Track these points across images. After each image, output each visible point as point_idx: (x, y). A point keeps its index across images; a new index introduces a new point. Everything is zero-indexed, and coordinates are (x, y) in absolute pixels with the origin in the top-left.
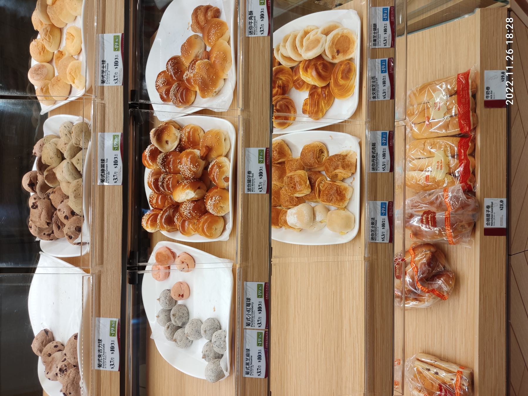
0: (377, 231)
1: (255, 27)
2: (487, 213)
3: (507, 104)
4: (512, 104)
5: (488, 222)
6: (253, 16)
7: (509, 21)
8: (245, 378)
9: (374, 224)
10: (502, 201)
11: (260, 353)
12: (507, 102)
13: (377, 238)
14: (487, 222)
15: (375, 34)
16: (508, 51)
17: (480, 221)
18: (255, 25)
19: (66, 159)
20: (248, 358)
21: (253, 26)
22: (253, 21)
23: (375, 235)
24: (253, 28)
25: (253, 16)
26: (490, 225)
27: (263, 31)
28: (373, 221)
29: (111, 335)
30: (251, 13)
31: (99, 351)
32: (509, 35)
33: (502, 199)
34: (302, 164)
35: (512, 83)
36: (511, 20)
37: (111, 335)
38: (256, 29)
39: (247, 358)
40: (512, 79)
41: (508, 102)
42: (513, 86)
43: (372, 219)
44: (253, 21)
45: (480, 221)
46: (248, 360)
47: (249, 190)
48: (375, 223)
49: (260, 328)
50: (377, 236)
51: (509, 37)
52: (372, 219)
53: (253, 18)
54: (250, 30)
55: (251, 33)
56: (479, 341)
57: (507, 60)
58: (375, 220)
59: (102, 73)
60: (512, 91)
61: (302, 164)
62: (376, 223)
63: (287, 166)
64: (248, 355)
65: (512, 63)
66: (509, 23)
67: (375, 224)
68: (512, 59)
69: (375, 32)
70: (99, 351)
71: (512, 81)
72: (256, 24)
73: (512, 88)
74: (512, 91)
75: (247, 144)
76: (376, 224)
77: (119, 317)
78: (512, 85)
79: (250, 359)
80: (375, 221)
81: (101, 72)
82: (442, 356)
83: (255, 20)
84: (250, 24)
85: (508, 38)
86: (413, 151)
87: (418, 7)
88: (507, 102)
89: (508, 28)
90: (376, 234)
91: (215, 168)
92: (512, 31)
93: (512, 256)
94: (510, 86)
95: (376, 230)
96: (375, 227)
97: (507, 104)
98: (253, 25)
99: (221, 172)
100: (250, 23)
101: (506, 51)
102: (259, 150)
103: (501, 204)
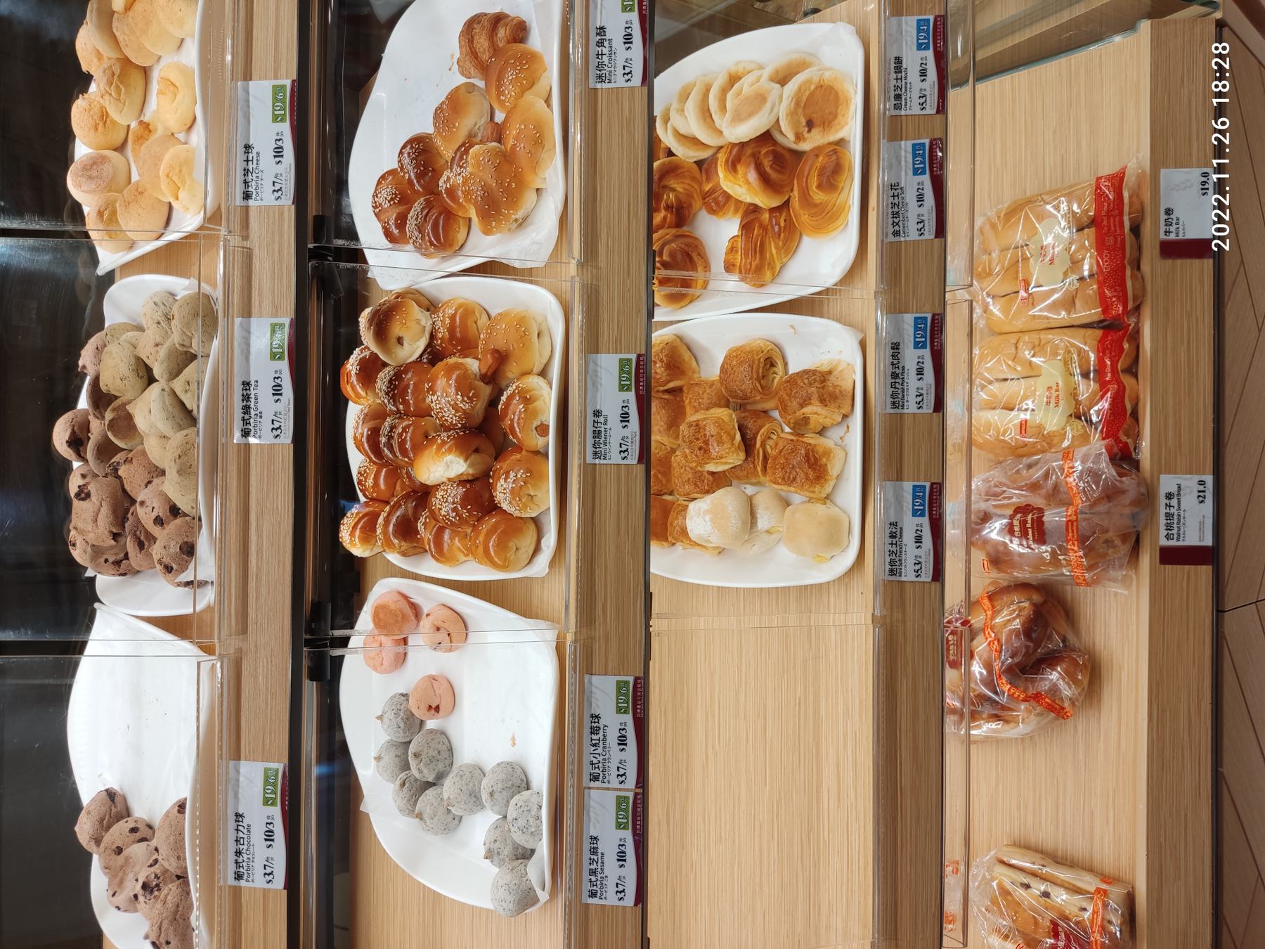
0: (904, 553)
1: (610, 66)
2: (1168, 511)
3: (1216, 249)
4: (1227, 248)
5: (1170, 532)
6: (607, 38)
7: (1220, 50)
8: (587, 905)
9: (895, 537)
10: (1202, 483)
11: (622, 845)
12: (1216, 245)
13: (903, 570)
14: (1166, 532)
15: (899, 81)
16: (1216, 123)
17: (1149, 531)
18: (610, 59)
19: (157, 381)
20: (595, 857)
21: (606, 62)
22: (606, 51)
23: (898, 564)
24: (606, 68)
25: (607, 38)
26: (1175, 538)
27: (630, 75)
28: (894, 530)
29: (266, 802)
30: (601, 31)
31: (237, 841)
32: (1220, 84)
33: (1203, 478)
34: (724, 393)
35: (1226, 199)
36: (1224, 48)
37: (266, 802)
38: (612, 69)
39: (593, 857)
40: (1228, 188)
41: (1217, 245)
42: (1229, 207)
43: (891, 524)
44: (606, 51)
45: (1149, 531)
46: (595, 863)
47: (596, 455)
48: (898, 533)
49: (622, 786)
50: (903, 565)
51: (1220, 88)
52: (891, 524)
53: (606, 44)
54: (598, 72)
55: (600, 78)
56: (1148, 817)
57: (1216, 143)
58: (898, 528)
59: (245, 175)
60: (1227, 218)
61: (724, 393)
62: (901, 534)
63: (687, 398)
64: (594, 851)
65: (1227, 150)
66: (1220, 56)
67: (898, 536)
68: (1227, 142)
69: (899, 77)
70: (237, 841)
71: (1228, 195)
72: (613, 58)
73: (1228, 211)
74: (1227, 218)
75: (592, 345)
76: (901, 536)
77: (286, 761)
78: (1227, 203)
79: (600, 861)
80: (899, 530)
81: (243, 172)
82: (1060, 853)
83: (611, 47)
84: (600, 57)
85: (1217, 90)
86: (989, 362)
87: (1002, 17)
88: (1216, 245)
89: (1216, 68)
90: (900, 560)
91: (515, 402)
92: (1228, 75)
93: (1226, 614)
94: (1221, 206)
95: (901, 552)
96: (898, 543)
97: (1216, 249)
98: (605, 59)
99: (531, 413)
100: (598, 55)
101: (1213, 122)
102: (621, 360)
103: (1201, 488)
